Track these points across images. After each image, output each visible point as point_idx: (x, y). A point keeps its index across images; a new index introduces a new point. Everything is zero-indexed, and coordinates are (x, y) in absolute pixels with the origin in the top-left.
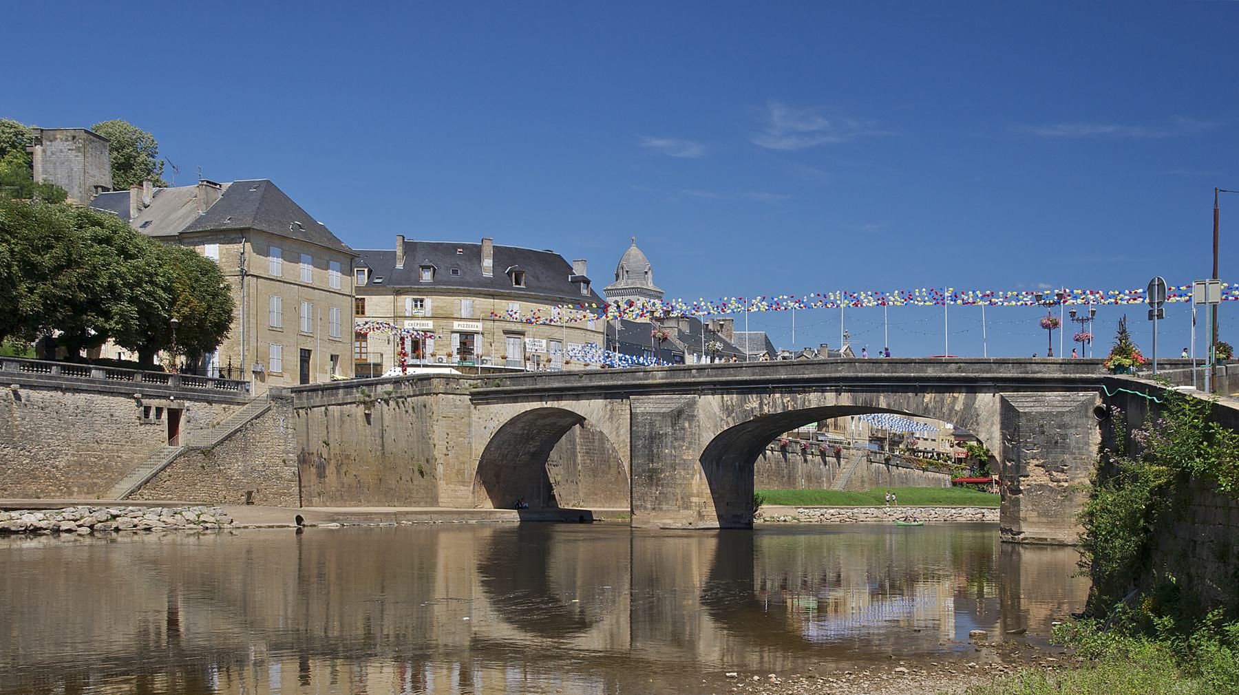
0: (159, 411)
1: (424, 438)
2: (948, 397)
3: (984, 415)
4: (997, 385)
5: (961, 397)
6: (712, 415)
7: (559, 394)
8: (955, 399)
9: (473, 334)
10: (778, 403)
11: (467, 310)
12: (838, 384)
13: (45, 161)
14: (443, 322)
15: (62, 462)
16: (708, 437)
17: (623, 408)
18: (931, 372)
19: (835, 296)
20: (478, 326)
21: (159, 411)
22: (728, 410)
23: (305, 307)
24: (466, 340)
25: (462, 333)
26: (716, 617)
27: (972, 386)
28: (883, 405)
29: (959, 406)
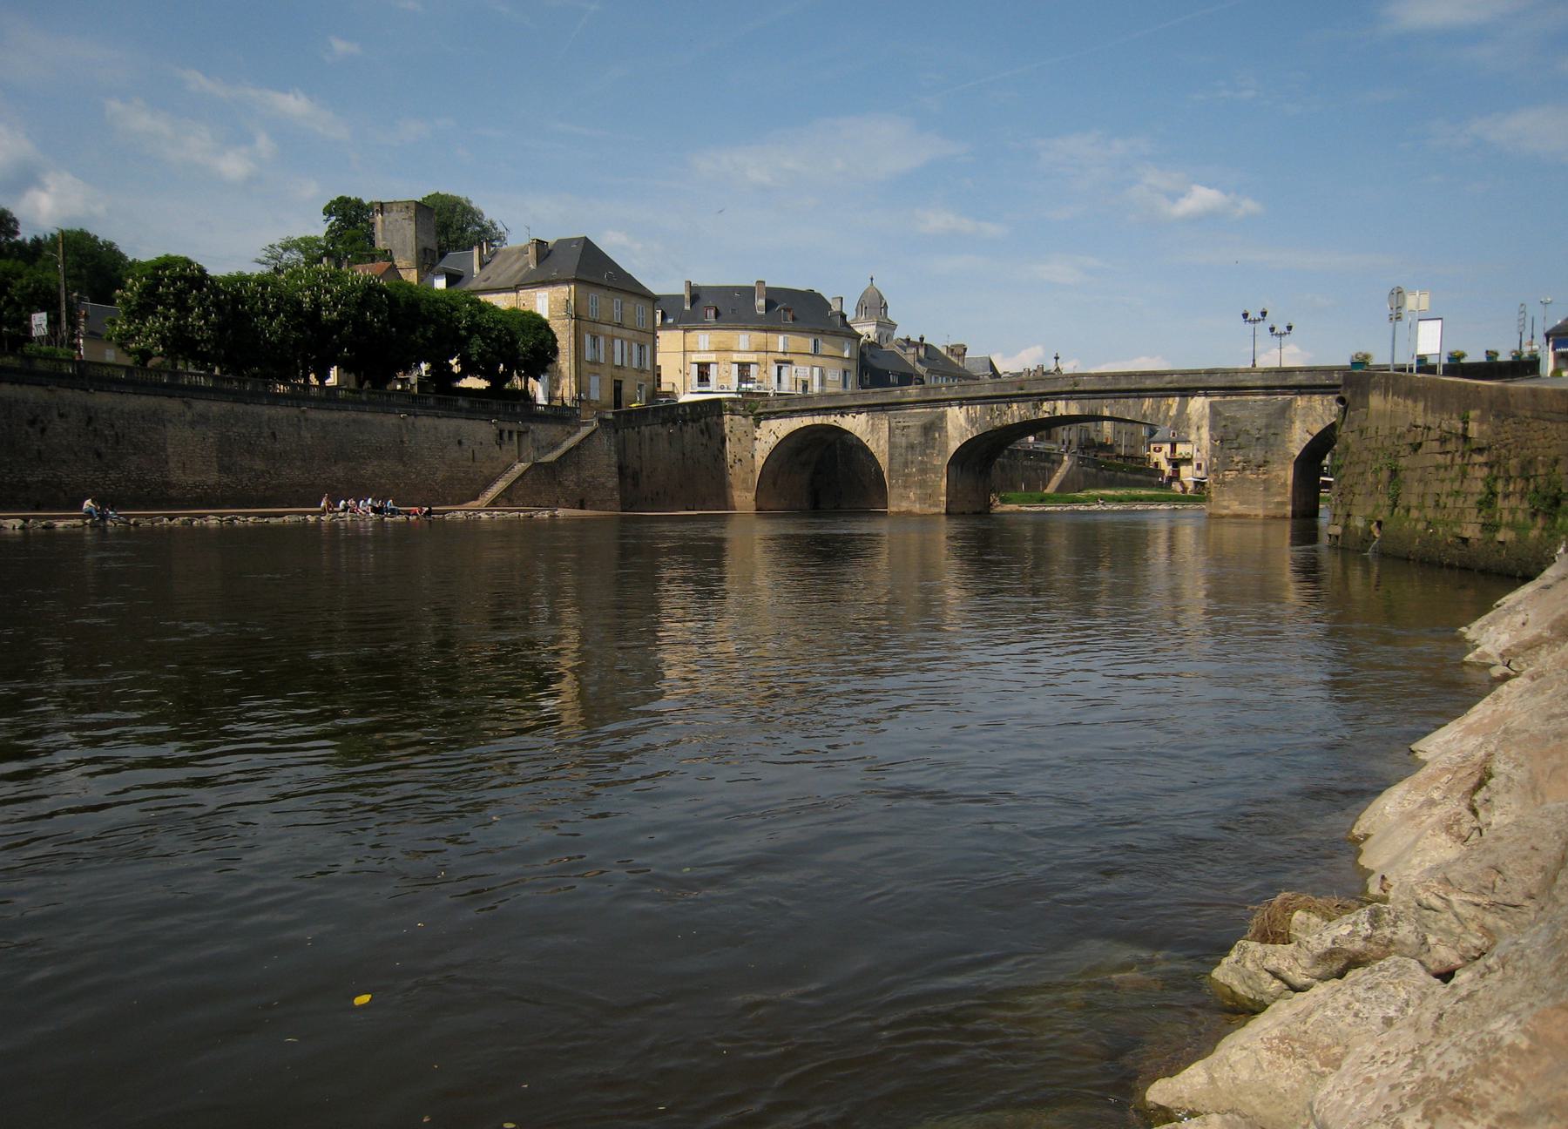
0: (510, 433)
1: (406, 205)
2: (1164, 402)
3: (1194, 419)
4: (1206, 391)
5: (1175, 402)
6: (959, 424)
7: (827, 411)
8: (1169, 406)
9: (749, 364)
10: (1016, 413)
11: (744, 342)
12: (1070, 395)
13: (384, 229)
14: (724, 355)
15: (440, 476)
16: (954, 445)
17: (884, 423)
18: (1149, 383)
19: (312, 376)
20: (712, 357)
21: (510, 433)
22: (971, 421)
23: (618, 343)
24: (744, 367)
25: (739, 364)
26: (537, 317)
27: (1186, 392)
28: (1106, 413)
29: (1173, 412)
